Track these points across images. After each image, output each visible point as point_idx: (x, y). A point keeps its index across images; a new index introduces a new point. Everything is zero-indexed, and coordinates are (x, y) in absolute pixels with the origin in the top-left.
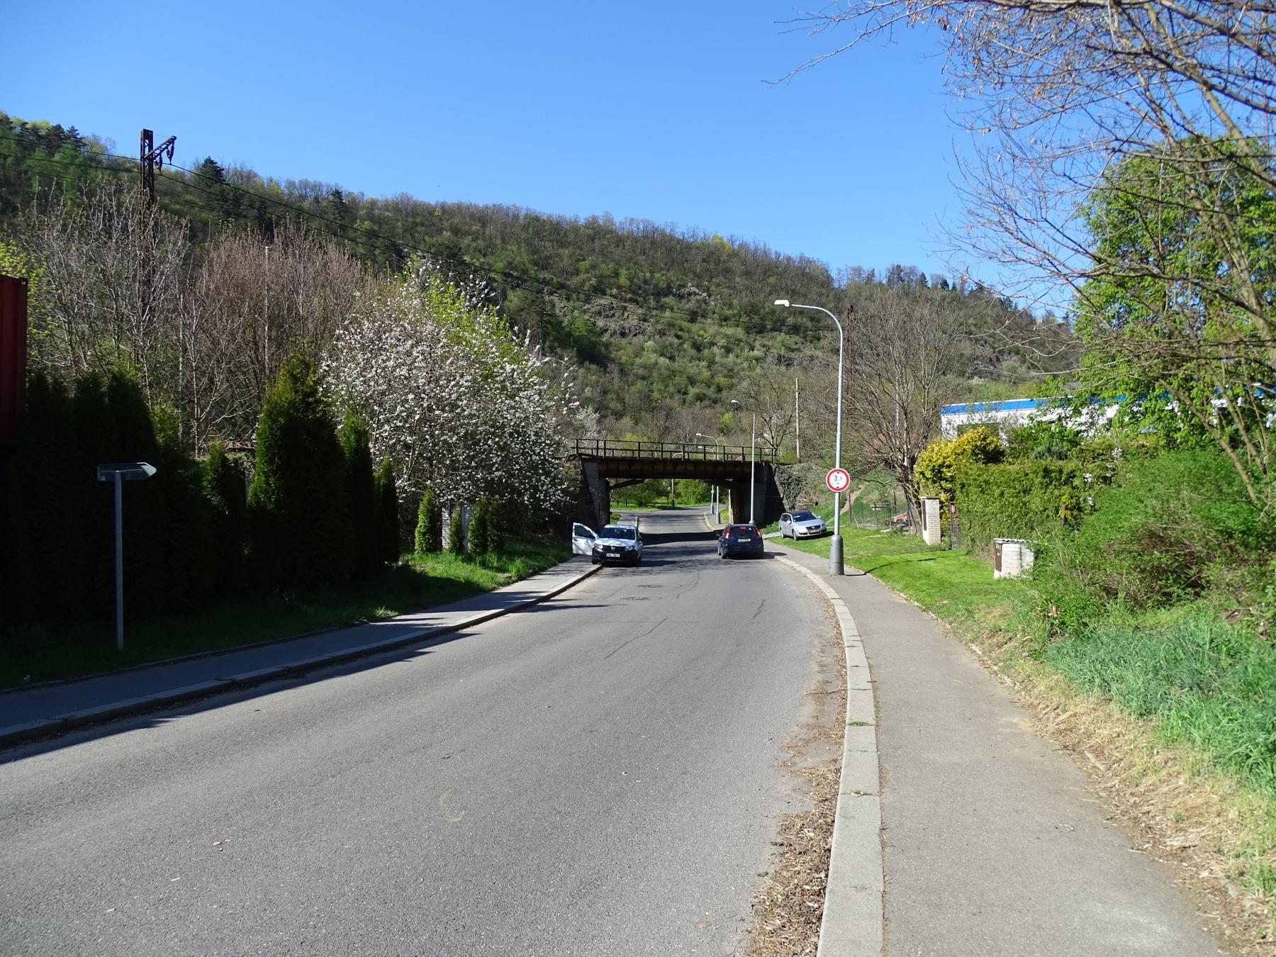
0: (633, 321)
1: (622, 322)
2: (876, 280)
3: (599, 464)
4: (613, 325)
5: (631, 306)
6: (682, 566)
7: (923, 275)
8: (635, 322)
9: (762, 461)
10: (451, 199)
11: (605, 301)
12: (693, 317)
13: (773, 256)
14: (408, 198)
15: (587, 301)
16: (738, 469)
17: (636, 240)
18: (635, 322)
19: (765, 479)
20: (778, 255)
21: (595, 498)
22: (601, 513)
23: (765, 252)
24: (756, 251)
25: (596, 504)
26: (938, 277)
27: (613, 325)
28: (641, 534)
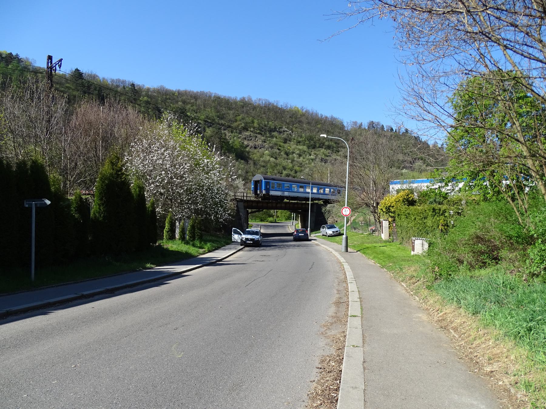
3: (244, 203)
4: (251, 144)
5: (259, 136)
7: (383, 126)
8: (261, 143)
10: (182, 88)
11: (248, 133)
15: (240, 133)
17: (261, 108)
18: (261, 143)
19: (315, 211)
22: (245, 224)
23: (316, 114)
24: (312, 114)
25: (243, 220)
26: (389, 127)
27: (251, 144)
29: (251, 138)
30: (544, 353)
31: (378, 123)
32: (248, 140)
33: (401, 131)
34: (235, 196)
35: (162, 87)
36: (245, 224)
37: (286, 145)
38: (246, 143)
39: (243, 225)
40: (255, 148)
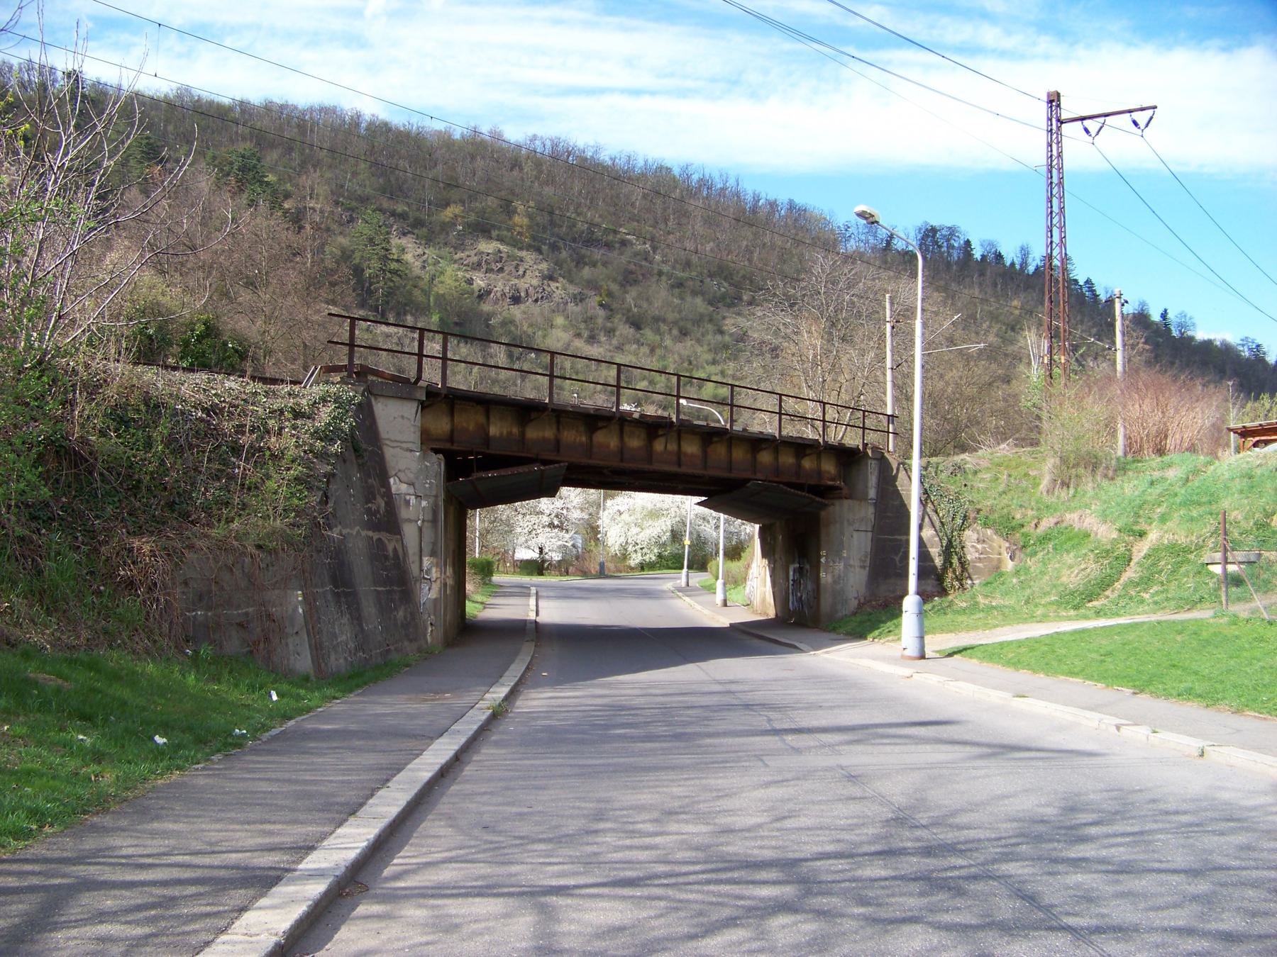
0: (530, 281)
1: (516, 281)
2: (899, 245)
3: (424, 406)
4: (501, 285)
5: (529, 256)
6: (821, 854)
7: (968, 243)
8: (535, 282)
9: (865, 445)
10: (255, 96)
11: (488, 247)
12: (629, 279)
13: (749, 198)
14: (188, 90)
15: (460, 247)
16: (807, 463)
17: (538, 163)
18: (535, 282)
19: (872, 493)
20: (756, 199)
21: (404, 513)
22: (427, 561)
23: (738, 194)
24: (723, 189)
25: (410, 532)
26: (991, 244)
27: (501, 285)
28: (1231, 574)
29: (499, 265)
30: (3, 528)
31: (952, 231)
32: (489, 271)
33: (1030, 260)
34: (351, 345)
35: (184, 92)
36: (427, 561)
37: (630, 297)
38: (480, 282)
39: (414, 569)
40: (516, 300)
